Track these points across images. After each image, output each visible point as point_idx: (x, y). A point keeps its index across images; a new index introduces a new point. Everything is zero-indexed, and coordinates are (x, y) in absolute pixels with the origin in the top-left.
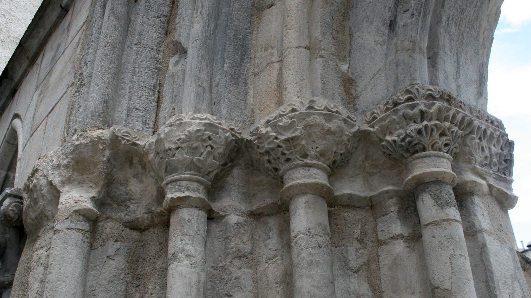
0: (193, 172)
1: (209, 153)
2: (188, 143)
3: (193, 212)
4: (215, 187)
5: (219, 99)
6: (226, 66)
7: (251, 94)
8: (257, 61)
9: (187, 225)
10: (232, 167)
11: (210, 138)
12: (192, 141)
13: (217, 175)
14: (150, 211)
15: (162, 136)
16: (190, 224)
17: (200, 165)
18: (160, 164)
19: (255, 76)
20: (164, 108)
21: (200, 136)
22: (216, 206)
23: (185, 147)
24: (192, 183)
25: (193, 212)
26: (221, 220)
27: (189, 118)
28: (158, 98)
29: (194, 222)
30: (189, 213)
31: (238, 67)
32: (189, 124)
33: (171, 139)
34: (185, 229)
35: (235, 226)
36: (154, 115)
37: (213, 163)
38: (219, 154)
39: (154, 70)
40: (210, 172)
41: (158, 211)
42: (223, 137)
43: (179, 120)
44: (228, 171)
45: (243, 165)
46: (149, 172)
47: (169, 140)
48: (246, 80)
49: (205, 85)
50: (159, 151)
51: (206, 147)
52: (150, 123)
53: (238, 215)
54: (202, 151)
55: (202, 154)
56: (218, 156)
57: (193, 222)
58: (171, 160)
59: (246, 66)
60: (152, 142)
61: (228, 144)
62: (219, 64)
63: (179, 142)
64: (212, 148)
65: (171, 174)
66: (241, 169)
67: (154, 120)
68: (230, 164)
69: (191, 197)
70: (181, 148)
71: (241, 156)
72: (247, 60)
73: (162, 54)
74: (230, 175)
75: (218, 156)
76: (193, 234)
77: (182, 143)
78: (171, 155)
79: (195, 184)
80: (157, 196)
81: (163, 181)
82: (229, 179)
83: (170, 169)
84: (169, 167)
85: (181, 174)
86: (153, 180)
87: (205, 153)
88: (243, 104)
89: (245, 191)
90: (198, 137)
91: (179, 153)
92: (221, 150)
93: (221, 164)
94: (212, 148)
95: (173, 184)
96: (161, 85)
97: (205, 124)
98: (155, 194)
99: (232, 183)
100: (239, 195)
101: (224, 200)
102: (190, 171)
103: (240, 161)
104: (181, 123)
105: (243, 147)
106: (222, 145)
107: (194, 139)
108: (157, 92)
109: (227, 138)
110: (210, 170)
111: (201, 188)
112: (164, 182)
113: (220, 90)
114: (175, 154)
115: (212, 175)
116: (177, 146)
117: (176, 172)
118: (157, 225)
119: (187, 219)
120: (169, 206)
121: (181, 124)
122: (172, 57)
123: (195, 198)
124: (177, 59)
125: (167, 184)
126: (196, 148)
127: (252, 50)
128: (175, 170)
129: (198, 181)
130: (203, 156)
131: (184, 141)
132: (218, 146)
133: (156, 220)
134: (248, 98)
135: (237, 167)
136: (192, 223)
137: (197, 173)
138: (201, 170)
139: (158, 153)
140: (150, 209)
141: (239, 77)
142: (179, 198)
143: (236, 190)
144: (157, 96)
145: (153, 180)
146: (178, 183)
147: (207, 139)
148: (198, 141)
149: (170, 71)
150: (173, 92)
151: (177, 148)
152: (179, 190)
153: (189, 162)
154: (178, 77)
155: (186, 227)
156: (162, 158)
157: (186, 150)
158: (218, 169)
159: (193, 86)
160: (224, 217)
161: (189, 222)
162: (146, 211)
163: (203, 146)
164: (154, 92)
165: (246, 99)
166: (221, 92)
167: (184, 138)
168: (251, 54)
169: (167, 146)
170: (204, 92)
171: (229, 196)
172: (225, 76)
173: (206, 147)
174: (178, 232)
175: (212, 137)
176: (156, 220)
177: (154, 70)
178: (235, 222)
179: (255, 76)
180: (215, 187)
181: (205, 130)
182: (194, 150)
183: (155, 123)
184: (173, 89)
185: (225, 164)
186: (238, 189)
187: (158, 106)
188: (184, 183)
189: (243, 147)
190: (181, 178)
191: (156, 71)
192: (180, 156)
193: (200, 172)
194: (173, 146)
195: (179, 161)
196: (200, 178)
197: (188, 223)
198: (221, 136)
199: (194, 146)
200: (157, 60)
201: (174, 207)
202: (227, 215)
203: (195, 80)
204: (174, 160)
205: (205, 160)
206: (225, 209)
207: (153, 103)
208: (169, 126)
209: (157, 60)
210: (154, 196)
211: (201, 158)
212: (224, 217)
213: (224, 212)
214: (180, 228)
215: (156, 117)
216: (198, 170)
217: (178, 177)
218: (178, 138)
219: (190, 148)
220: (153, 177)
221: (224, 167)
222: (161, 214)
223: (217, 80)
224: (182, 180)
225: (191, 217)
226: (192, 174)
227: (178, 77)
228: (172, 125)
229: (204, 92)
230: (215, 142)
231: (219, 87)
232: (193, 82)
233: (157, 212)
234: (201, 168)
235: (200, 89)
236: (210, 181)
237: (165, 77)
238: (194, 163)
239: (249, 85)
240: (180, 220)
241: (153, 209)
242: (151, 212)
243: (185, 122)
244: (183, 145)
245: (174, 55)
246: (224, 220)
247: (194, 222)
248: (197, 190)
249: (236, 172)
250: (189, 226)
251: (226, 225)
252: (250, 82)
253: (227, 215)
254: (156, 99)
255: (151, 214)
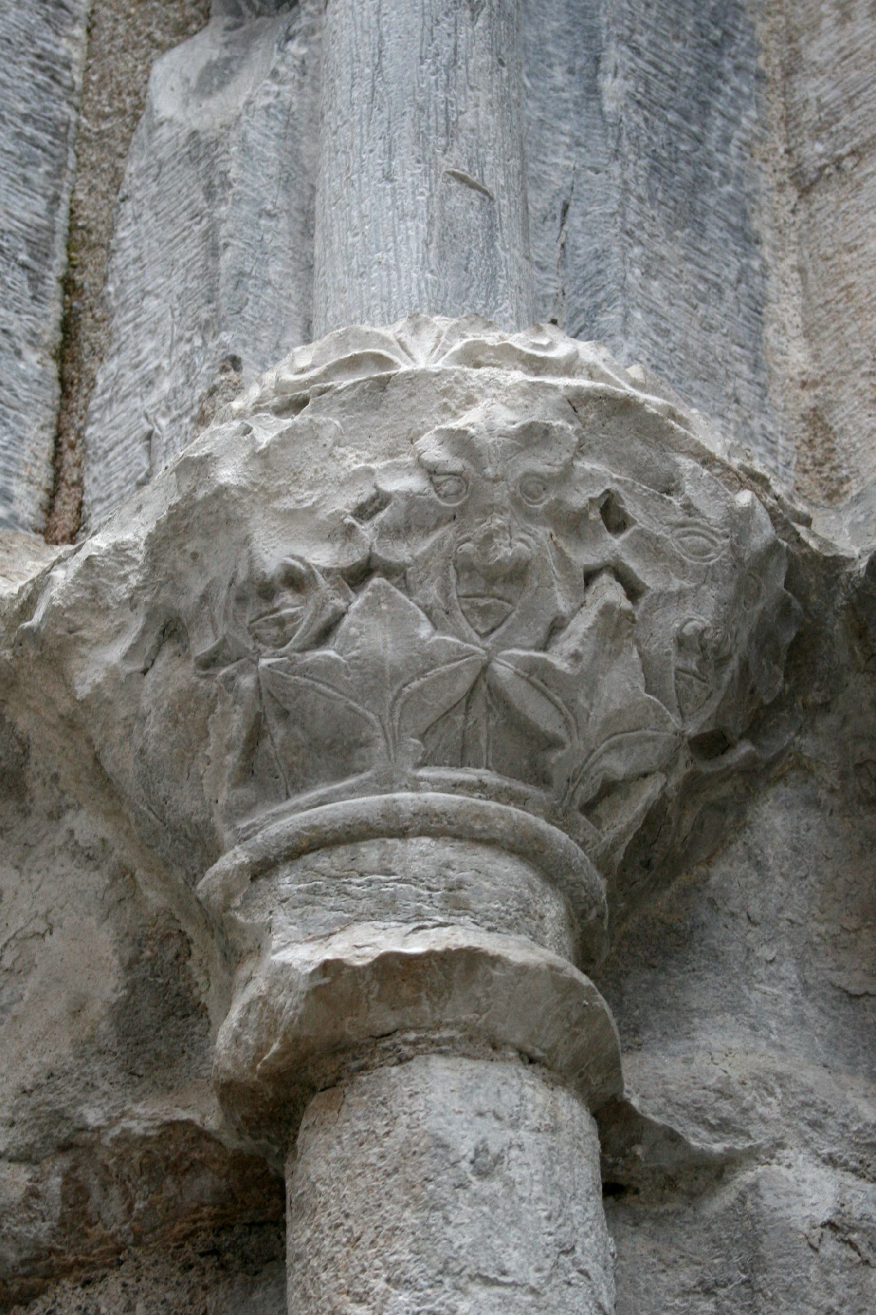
0: (490, 778)
1: (615, 628)
2: (447, 532)
3: (510, 1098)
4: (639, 922)
5: (585, 302)
6: (613, 87)
7: (786, 308)
8: (811, 88)
9: (478, 1199)
10: (755, 777)
11: (613, 516)
12: (488, 510)
13: (655, 818)
14: (63, 1132)
15: (227, 474)
16: (496, 1185)
17: (541, 715)
18: (189, 716)
19: (805, 192)
20: (131, 377)
21: (546, 482)
22: (655, 1080)
23: (422, 561)
24: (483, 856)
25: (510, 1098)
26: (693, 1197)
27: (439, 348)
28: (69, 326)
29: (525, 1169)
30: (480, 1100)
31: (685, 115)
32: (452, 395)
33: (309, 497)
34: (463, 1229)
35: (830, 1248)
36: (38, 442)
37: (626, 708)
38: (681, 642)
39: (29, 130)
40: (610, 788)
41: (137, 1128)
42: (713, 513)
43: (354, 363)
44: (720, 808)
45: (831, 779)
46: (55, 815)
47: (288, 503)
48: (745, 215)
49: (495, 180)
50: (185, 604)
51: (590, 576)
52: (18, 489)
53: (831, 1161)
54: (563, 604)
55: (556, 627)
56: (676, 661)
57: (516, 1173)
58: (306, 671)
59: (734, 121)
60: (119, 550)
61: (748, 573)
62: (559, 76)
63: (366, 530)
64: (633, 591)
65: (297, 785)
66: (814, 803)
67: (43, 474)
68: (744, 749)
69: (495, 960)
70: (390, 571)
71: (815, 697)
72: (735, 81)
73: (79, 31)
74: (737, 849)
75: (676, 661)
76: (533, 1278)
77: (399, 532)
78: (300, 633)
79: (508, 870)
80: (123, 1012)
81: (214, 853)
82: (728, 873)
83: (295, 738)
84: (279, 732)
85: (386, 783)
86: (97, 880)
87: (582, 624)
88: (744, 369)
89: (855, 982)
90: (531, 487)
91: (371, 608)
92: (699, 616)
93: (692, 730)
94: (633, 591)
95: (323, 862)
96: (84, 241)
97: (576, 402)
98: (108, 987)
99: (755, 908)
100: (811, 1012)
101: (702, 1039)
102: (461, 760)
103: (808, 745)
104: (383, 384)
105: (837, 627)
106: (708, 576)
107: (500, 494)
108: (52, 285)
109: (738, 521)
110: (618, 766)
111: (552, 908)
112: (234, 858)
113: (584, 245)
114: (339, 616)
115: (624, 817)
116: (354, 556)
117: (344, 772)
118: (116, 1257)
119: (466, 1148)
120: (293, 1043)
121: (378, 387)
122: (163, 48)
123: (523, 970)
124: (215, 54)
125: (263, 869)
126: (518, 573)
127: (762, 28)
128: (338, 753)
129: (525, 849)
130: (570, 642)
131: (414, 519)
132: (676, 584)
133: (111, 1212)
134: (769, 331)
135: (784, 791)
136: (510, 1184)
137: (520, 787)
138: (555, 756)
139: (170, 630)
140: (59, 1116)
141: (699, 183)
142: (391, 967)
143: (788, 969)
144: (54, 311)
145: (97, 880)
146: (370, 853)
147: (594, 515)
148: (530, 516)
149: (165, 133)
150: (214, 252)
151: (357, 576)
152: (386, 908)
153: (462, 686)
154: (246, 150)
155: (463, 1213)
156: (210, 662)
157: (433, 592)
158: (667, 770)
159: (409, 174)
160: (719, 1170)
161: (483, 1173)
162: (21, 1137)
163: (565, 563)
164: (36, 280)
165: (757, 336)
166: (598, 256)
167: (410, 497)
168: (754, 49)
169: (273, 553)
170: (492, 229)
171: (736, 1008)
172: (616, 154)
173: (590, 576)
174: (401, 1251)
175: (631, 507)
176: (114, 1208)
177: (29, 130)
178: (824, 1214)
179: (805, 192)
180: (639, 922)
181: (581, 450)
182: (494, 588)
183: (53, 494)
184: (210, 234)
185: (711, 744)
186: (801, 962)
187: (64, 382)
188: (420, 853)
189: (837, 627)
190: (390, 813)
191: (45, 138)
192: (373, 631)
193: (543, 780)
194: (322, 556)
195: (375, 677)
196: (543, 825)
197: (476, 1184)
198: (700, 503)
199: (504, 551)
200: (49, 67)
201: (339, 1048)
202: (752, 1154)
203: (421, 138)
204: (329, 668)
205: (589, 681)
206: (726, 1108)
207: (32, 357)
208: (279, 411)
209: (49, 67)
210: (96, 1009)
211: (557, 659)
212: (719, 1170)
213: (723, 1127)
214: (411, 1218)
215: (57, 456)
216: (528, 755)
217: (366, 804)
218: (363, 493)
219: (465, 568)
220: (89, 857)
221: (707, 768)
222: (173, 1152)
223: (557, 180)
224: (403, 834)
225: (497, 1138)
226: (480, 787)
227: (246, 150)
228: (298, 405)
229: (492, 229)
230: (650, 547)
231: (575, 220)
232: (405, 154)
233: (125, 1138)
234: (553, 743)
235: (460, 200)
236: (602, 864)
237: (116, 180)
238: (498, 698)
239: (766, 251)
240: (409, 1152)
241: (93, 1116)
242: (65, 1148)
243: (413, 378)
244: (401, 553)
245: (182, 31)
246: (726, 1197)
247: (525, 1169)
248: (520, 920)
249: (777, 822)
250: (491, 1201)
251: (753, 1240)
252: (768, 235)
253: (752, 1154)
254: (50, 333)
255: (64, 1162)
